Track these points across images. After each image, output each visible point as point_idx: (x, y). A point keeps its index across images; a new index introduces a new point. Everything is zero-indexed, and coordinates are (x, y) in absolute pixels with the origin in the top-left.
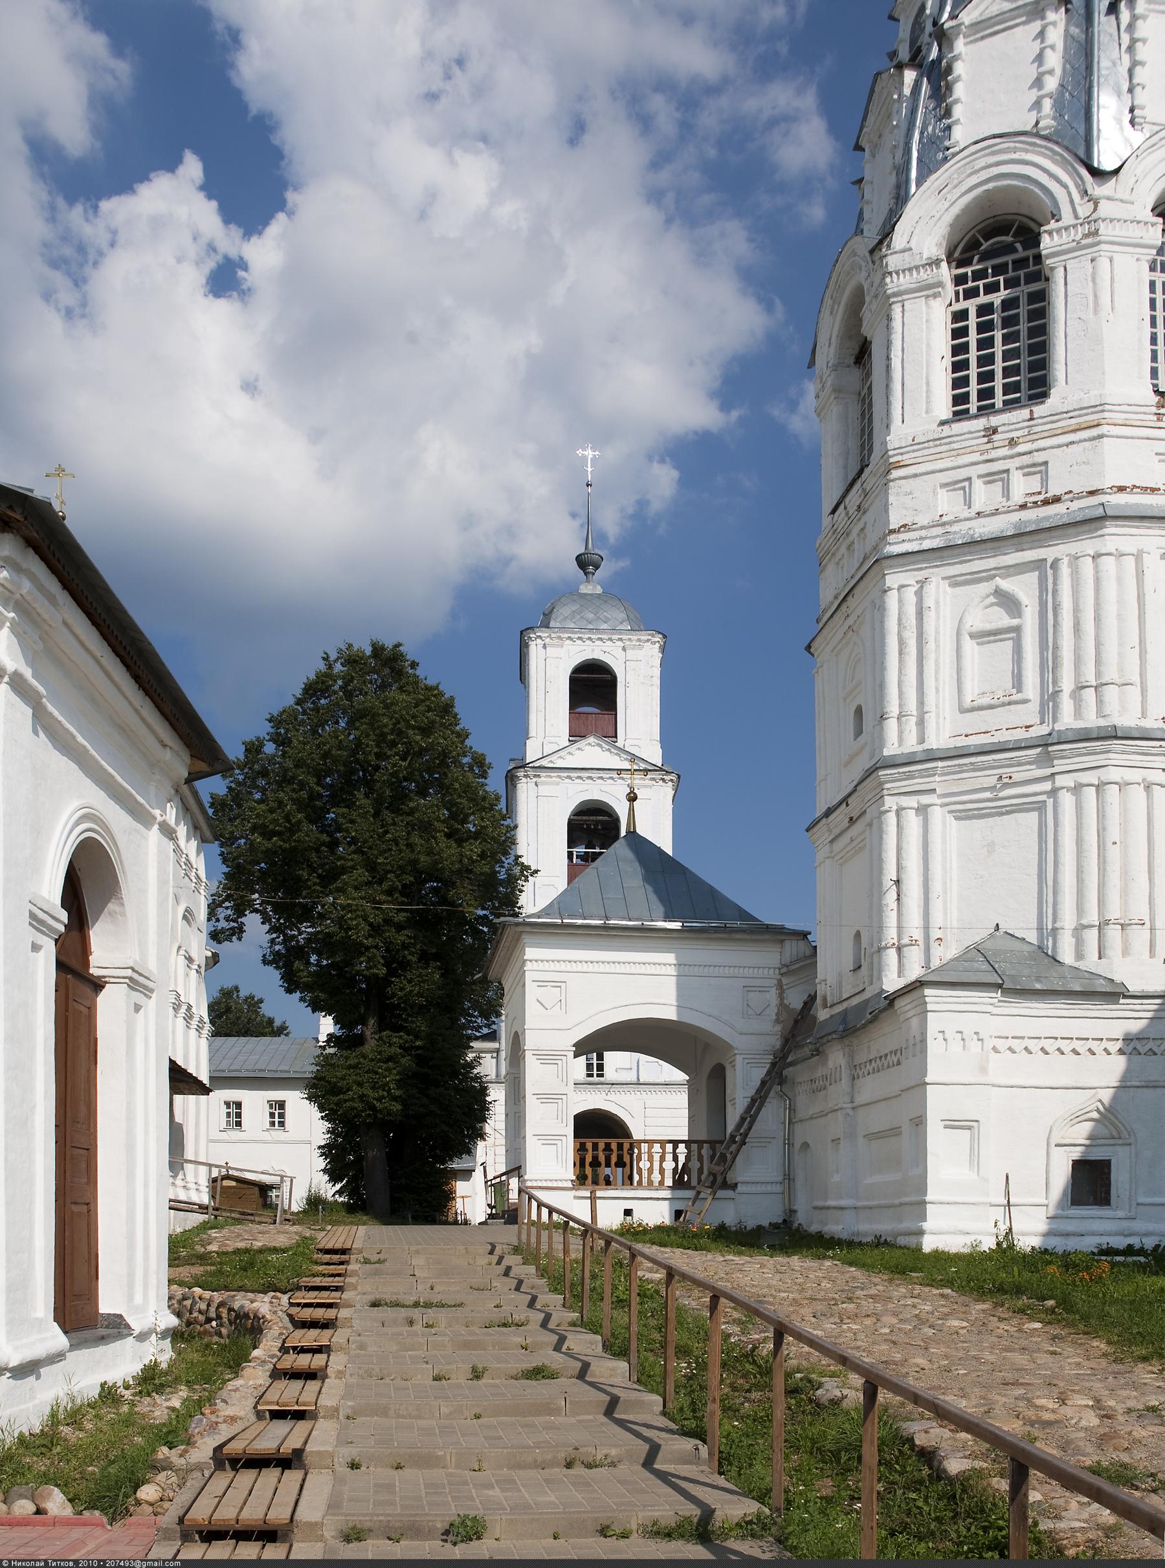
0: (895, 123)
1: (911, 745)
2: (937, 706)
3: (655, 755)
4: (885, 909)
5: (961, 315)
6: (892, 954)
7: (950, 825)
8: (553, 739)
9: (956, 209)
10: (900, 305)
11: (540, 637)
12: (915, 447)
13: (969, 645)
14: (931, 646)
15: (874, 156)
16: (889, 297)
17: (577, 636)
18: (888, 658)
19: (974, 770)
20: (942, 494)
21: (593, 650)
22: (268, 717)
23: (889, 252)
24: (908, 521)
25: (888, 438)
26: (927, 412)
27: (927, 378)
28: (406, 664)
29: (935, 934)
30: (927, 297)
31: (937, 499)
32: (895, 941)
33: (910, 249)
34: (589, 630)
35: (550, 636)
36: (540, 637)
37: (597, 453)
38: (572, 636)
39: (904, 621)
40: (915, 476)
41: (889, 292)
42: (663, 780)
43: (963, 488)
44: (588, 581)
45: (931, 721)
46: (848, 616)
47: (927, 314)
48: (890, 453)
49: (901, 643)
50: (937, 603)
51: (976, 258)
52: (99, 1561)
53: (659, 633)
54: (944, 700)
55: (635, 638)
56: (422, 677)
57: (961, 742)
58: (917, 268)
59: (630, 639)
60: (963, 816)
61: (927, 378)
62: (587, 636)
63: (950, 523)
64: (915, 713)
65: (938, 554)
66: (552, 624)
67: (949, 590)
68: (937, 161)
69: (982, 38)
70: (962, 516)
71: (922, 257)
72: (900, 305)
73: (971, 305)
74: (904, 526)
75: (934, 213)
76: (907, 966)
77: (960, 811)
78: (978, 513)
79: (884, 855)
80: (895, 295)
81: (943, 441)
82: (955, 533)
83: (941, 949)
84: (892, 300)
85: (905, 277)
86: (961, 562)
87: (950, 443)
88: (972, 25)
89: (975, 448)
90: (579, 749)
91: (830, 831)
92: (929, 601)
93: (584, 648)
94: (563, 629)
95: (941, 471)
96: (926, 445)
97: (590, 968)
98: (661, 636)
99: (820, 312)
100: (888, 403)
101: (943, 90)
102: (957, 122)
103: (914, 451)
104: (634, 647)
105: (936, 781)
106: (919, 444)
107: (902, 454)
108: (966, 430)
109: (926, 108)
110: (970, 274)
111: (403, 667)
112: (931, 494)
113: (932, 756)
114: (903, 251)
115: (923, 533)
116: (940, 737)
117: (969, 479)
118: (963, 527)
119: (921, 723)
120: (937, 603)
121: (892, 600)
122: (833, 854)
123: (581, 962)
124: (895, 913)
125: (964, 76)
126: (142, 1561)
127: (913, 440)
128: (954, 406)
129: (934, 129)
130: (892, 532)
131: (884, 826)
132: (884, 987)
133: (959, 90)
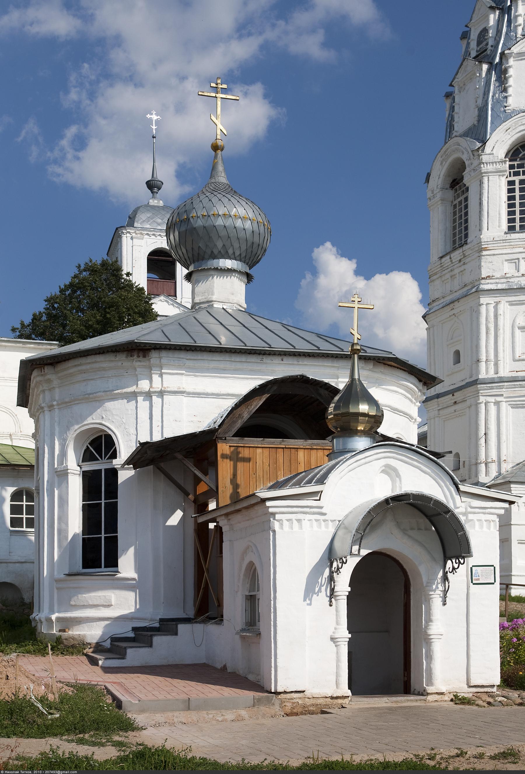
0: (478, 87)
1: (491, 374)
2: (504, 358)
4: (480, 446)
5: (511, 183)
6: (483, 465)
7: (509, 410)
9: (513, 139)
10: (487, 177)
11: (129, 233)
12: (494, 242)
13: (518, 332)
14: (501, 331)
15: (460, 92)
16: (482, 173)
17: (152, 233)
18: (481, 335)
19: (521, 387)
20: (506, 263)
21: (162, 242)
22: (45, 298)
23: (483, 154)
24: (491, 275)
25: (481, 237)
26: (499, 227)
27: (499, 212)
29: (503, 458)
30: (499, 175)
31: (504, 266)
32: (484, 460)
33: (493, 154)
35: (135, 232)
36: (129, 233)
37: (159, 117)
38: (149, 233)
39: (489, 319)
40: (494, 255)
41: (482, 171)
43: (515, 263)
44: (153, 197)
45: (501, 364)
46: (453, 309)
47: (499, 183)
48: (483, 243)
49: (487, 329)
50: (504, 312)
51: (518, 159)
54: (506, 356)
56: (134, 282)
57: (514, 374)
58: (496, 162)
60: (515, 407)
61: (499, 212)
62: (158, 234)
63: (510, 278)
64: (493, 360)
65: (505, 291)
66: (136, 225)
67: (509, 307)
68: (501, 111)
69: (521, 60)
70: (515, 275)
71: (498, 158)
72: (487, 177)
73: (517, 179)
74: (489, 276)
75: (504, 139)
76: (490, 472)
77: (514, 405)
78: (523, 275)
79: (479, 422)
80: (485, 173)
81: (507, 241)
82: (512, 282)
83: (505, 464)
84: (483, 175)
85: (490, 166)
86: (515, 296)
87: (510, 242)
88: (517, 53)
89: (521, 246)
91: (438, 405)
92: (500, 312)
94: (143, 229)
95: (506, 254)
96: (499, 242)
99: (434, 162)
100: (480, 220)
101: (503, 79)
102: (510, 96)
103: (493, 244)
105: (503, 391)
106: (496, 241)
107: (488, 244)
108: (517, 238)
109: (495, 85)
110: (516, 165)
112: (501, 264)
113: (502, 380)
114: (490, 154)
115: (497, 281)
116: (504, 372)
117: (518, 259)
118: (516, 280)
119: (496, 365)
120: (504, 312)
121: (483, 309)
122: (440, 416)
124: (484, 448)
125: (513, 76)
127: (493, 239)
128: (508, 223)
129: (499, 96)
130: (483, 279)
131: (479, 409)
132: (479, 480)
133: (511, 82)
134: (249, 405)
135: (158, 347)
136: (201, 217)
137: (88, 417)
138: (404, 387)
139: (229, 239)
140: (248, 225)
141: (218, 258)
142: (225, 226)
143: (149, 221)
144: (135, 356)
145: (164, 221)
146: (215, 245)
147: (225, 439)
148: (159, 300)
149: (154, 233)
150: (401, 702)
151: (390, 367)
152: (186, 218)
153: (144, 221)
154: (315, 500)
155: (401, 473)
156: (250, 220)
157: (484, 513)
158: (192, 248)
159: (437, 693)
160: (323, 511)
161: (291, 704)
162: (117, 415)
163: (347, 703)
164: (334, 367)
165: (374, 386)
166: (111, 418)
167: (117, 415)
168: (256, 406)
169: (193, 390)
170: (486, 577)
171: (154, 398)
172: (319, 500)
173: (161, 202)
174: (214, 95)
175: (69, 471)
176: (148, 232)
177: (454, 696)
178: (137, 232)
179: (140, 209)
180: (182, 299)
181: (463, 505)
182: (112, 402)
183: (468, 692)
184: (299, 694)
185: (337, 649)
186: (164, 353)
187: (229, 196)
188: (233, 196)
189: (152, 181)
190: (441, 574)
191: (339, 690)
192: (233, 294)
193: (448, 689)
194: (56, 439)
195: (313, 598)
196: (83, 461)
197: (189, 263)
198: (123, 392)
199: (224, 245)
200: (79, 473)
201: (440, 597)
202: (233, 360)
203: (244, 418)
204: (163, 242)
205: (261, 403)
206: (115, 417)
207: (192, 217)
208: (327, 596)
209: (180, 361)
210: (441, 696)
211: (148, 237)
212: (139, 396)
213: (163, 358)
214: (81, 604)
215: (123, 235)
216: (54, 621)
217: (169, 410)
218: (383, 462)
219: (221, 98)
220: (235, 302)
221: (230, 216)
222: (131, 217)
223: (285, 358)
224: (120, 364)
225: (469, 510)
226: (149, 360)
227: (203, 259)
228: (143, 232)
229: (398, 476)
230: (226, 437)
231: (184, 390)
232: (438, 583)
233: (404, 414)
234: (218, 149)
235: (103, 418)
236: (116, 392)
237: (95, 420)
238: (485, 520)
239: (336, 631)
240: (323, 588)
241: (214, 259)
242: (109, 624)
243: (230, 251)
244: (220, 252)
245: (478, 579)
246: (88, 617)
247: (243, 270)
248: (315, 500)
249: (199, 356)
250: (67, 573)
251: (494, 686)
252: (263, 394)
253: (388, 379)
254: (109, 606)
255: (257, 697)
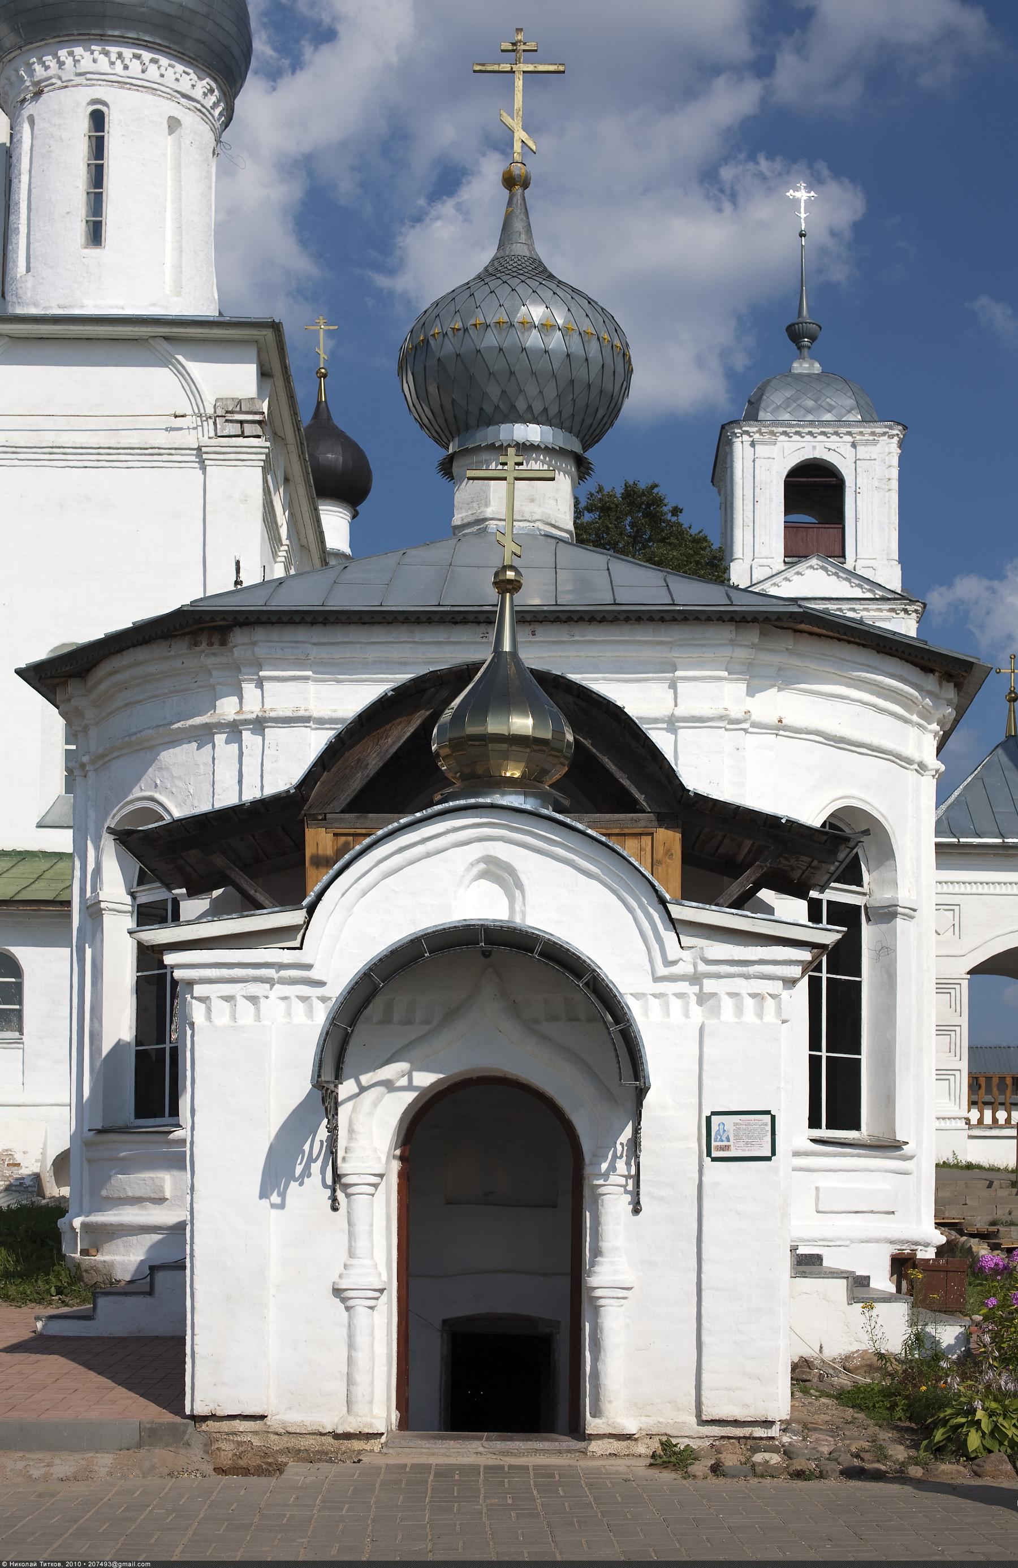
3: (892, 578)
8: (764, 561)
17: (794, 430)
21: (814, 447)
28: (665, 509)
34: (816, 426)
36: (747, 433)
38: (788, 430)
42: (906, 611)
52: (83, 1562)
53: (899, 424)
55: (869, 430)
56: (686, 526)
59: (861, 433)
62: (807, 430)
66: (762, 415)
90: (798, 573)
93: (804, 445)
94: (776, 423)
97: (986, 889)
98: (900, 428)
104: (867, 443)
111: (663, 514)
123: (975, 883)
126: (118, 1562)
134: (382, 737)
135: (252, 620)
136: (450, 333)
137: (134, 787)
138: (866, 686)
139: (513, 376)
140: (556, 341)
141: (497, 423)
142: (501, 350)
143: (788, 406)
144: (204, 646)
145: (819, 403)
146: (484, 394)
147: (325, 819)
148: (807, 568)
149: (798, 429)
150: (519, 1454)
151: (816, 638)
152: (423, 340)
153: (778, 407)
154: (288, 948)
155: (523, 878)
156: (559, 329)
157: (747, 977)
158: (441, 405)
159: (611, 1436)
160: (314, 974)
161: (232, 1446)
162: (179, 778)
163: (377, 1449)
164: (662, 643)
165: (772, 686)
166: (169, 786)
167: (179, 778)
168: (400, 738)
169: (329, 713)
170: (747, 1143)
171: (246, 735)
172: (301, 948)
173: (817, 365)
174: (507, 67)
175: (103, 905)
176: (785, 429)
177: (662, 1444)
178: (764, 430)
179: (772, 384)
180: (856, 561)
181: (686, 955)
182: (171, 751)
183: (700, 1435)
184: (252, 1423)
185: (350, 1317)
186: (260, 634)
187: (534, 284)
188: (559, 285)
189: (798, 324)
190: (628, 1133)
191: (350, 1419)
192: (532, 500)
193: (644, 1426)
194: (89, 838)
195: (289, 1191)
196: (140, 883)
197: (446, 440)
198: (187, 725)
199: (504, 392)
200: (130, 908)
201: (626, 1192)
202: (417, 640)
203: (370, 767)
204: (818, 448)
205: (411, 730)
206: (177, 782)
207: (433, 335)
208: (325, 1185)
209: (297, 648)
210: (625, 1443)
211: (787, 438)
212: (217, 733)
213: (260, 644)
214: (115, 1196)
215: (735, 440)
216: (78, 1230)
217: (276, 761)
218: (477, 851)
219: (524, 72)
220: (536, 517)
221: (512, 325)
222: (753, 400)
223: (540, 629)
224: (178, 663)
225: (702, 967)
226: (232, 651)
227: (467, 428)
228: (775, 430)
229: (519, 885)
230: (325, 814)
231: (307, 714)
232: (615, 1157)
233: (873, 750)
234: (515, 185)
235: (156, 786)
236: (176, 726)
237: (145, 791)
238: (750, 995)
239: (347, 1272)
240: (316, 1167)
241: (489, 425)
242: (160, 1242)
243: (521, 405)
244: (497, 407)
245: (727, 1148)
246: (122, 1225)
247: (560, 443)
248: (288, 948)
249: (339, 634)
250: (100, 1127)
251: (773, 1423)
252: (416, 711)
253: (812, 666)
254: (161, 1200)
255: (148, 1426)
